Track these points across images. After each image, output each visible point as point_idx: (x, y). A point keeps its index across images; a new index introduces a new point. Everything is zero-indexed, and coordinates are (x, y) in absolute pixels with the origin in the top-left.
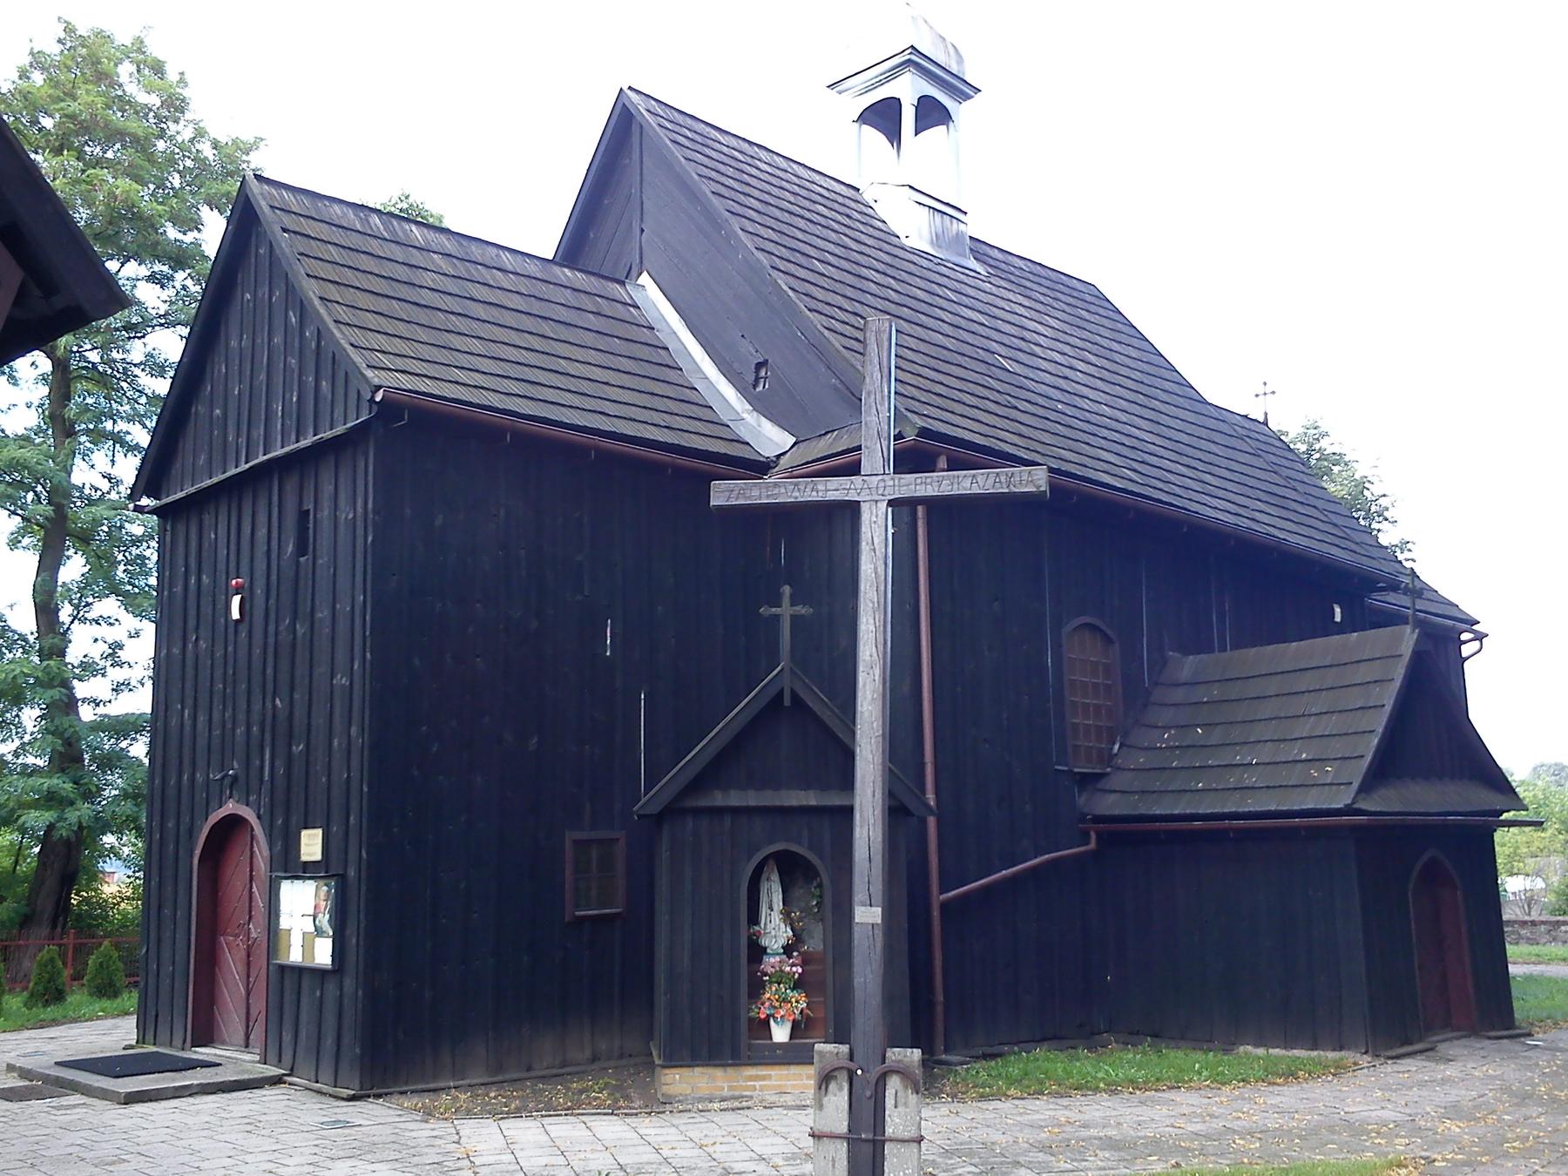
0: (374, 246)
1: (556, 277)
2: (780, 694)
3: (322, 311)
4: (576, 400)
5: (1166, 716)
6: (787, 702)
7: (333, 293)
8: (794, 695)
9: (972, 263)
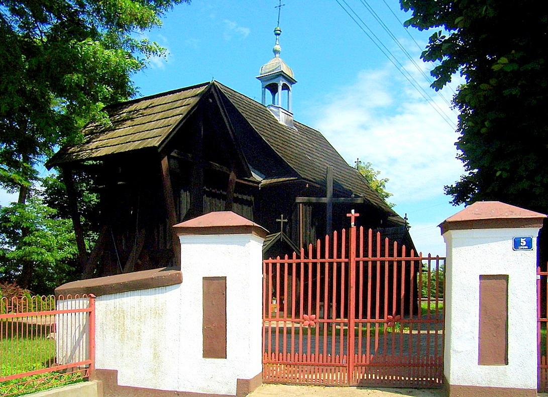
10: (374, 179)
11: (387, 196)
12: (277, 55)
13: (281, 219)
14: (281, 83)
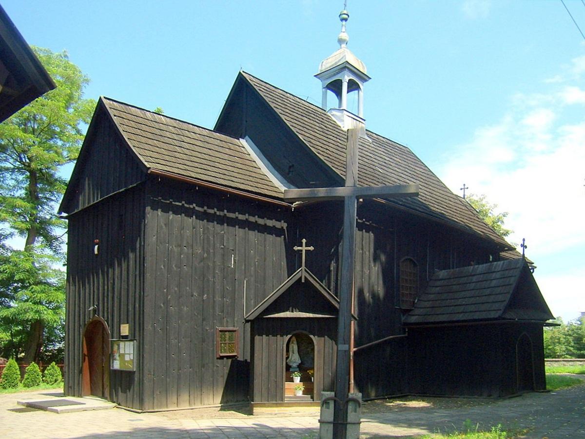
0: (149, 123)
1: (214, 136)
2: (301, 278)
3: (129, 143)
4: (222, 176)
5: (434, 290)
6: (303, 281)
7: (133, 137)
8: (305, 277)
9: (366, 137)
10: (489, 215)
11: (506, 233)
12: (343, 45)
13: (302, 246)
14: (346, 78)
